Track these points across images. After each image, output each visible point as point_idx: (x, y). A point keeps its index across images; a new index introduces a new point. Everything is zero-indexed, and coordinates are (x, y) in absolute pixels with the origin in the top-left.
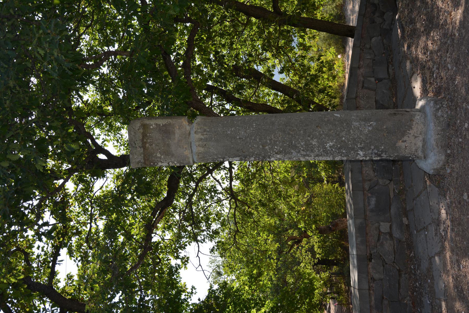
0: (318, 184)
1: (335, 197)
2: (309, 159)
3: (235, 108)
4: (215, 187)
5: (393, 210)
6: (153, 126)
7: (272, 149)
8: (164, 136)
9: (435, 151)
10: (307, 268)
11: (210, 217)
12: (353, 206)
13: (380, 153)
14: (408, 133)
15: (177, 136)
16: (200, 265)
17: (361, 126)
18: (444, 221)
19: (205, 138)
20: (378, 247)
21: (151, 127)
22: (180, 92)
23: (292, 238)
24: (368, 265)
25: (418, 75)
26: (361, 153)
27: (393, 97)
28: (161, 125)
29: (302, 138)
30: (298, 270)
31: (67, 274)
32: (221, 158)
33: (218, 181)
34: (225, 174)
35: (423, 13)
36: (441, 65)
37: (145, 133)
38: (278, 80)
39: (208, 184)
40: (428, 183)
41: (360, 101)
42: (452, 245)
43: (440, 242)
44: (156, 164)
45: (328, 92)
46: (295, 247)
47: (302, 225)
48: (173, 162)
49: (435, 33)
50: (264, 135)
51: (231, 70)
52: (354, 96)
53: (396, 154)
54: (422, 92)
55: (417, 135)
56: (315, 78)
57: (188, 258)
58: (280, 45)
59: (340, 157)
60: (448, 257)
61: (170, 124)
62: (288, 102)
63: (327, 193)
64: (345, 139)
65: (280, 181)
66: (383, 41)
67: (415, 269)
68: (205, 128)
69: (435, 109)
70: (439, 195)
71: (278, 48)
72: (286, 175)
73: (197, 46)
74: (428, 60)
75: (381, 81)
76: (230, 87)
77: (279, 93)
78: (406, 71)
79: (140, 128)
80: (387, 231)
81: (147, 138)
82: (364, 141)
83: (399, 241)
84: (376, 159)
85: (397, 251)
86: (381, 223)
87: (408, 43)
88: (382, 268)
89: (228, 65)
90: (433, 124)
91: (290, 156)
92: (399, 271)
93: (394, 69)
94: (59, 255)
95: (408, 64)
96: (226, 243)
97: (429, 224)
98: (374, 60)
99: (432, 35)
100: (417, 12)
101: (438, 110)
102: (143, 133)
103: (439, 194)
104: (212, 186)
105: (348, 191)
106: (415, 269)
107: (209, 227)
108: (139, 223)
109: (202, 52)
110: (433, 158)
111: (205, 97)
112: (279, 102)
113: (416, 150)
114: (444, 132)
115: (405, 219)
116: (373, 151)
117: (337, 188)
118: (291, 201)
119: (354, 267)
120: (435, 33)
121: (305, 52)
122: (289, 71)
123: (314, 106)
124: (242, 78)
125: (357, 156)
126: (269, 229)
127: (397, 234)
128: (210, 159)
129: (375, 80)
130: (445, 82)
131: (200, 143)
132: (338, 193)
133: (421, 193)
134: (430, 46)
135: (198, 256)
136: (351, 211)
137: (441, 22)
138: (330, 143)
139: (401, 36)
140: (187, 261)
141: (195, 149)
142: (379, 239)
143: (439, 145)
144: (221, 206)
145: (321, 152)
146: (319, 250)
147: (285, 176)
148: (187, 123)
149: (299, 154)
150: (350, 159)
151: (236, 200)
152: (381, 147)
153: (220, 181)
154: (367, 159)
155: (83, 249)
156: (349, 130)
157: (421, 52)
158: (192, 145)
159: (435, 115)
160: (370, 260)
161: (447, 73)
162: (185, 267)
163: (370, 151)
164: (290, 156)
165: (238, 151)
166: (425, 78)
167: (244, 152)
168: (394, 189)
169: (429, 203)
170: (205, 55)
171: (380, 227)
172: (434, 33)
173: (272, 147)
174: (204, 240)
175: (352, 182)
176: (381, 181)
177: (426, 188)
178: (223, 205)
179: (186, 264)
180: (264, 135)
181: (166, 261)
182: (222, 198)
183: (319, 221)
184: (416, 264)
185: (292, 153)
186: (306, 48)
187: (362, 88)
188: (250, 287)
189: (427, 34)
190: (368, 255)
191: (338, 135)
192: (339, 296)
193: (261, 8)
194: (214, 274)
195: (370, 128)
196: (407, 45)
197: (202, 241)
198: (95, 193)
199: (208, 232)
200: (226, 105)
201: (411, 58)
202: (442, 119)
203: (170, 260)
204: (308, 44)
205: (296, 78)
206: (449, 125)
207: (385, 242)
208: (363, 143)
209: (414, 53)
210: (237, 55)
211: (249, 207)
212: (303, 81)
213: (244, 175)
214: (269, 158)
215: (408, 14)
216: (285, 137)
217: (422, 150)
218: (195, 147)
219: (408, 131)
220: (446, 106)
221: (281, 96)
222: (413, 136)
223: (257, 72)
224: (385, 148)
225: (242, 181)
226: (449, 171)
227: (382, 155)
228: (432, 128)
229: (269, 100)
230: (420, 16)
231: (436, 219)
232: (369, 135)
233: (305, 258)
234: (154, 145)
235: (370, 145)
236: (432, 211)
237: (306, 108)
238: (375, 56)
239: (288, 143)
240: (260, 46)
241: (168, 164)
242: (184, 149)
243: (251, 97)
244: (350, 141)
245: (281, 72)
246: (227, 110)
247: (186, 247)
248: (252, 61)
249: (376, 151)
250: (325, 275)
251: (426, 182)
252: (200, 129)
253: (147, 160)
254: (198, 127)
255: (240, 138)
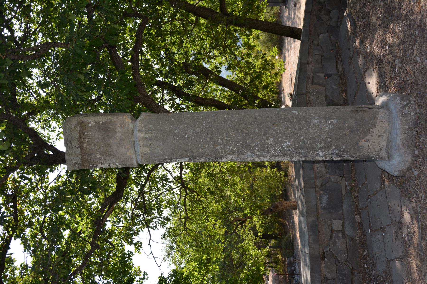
0: (258, 169)
1: (274, 181)
2: (264, 160)
3: (185, 102)
4: (166, 176)
5: (345, 207)
6: (91, 124)
7: (224, 149)
8: (104, 135)
9: (400, 151)
10: (249, 245)
11: (163, 203)
12: (304, 204)
13: (342, 153)
14: (372, 131)
15: (118, 134)
16: (151, 253)
17: (321, 124)
18: (408, 226)
19: (149, 137)
20: (331, 245)
21: (90, 125)
22: (123, 87)
23: (237, 219)
24: (321, 264)
25: (374, 70)
26: (321, 153)
27: (343, 93)
28: (101, 123)
29: (256, 137)
30: (242, 247)
31: (20, 264)
32: (168, 159)
33: (169, 172)
34: (176, 164)
35: (380, 6)
36: (405, 59)
37: (82, 132)
38: (225, 77)
39: (160, 173)
40: (386, 183)
41: (311, 97)
42: (422, 254)
43: (402, 246)
44: (95, 166)
45: (272, 88)
46: (240, 226)
47: (248, 211)
48: (114, 164)
49: (396, 26)
50: (215, 134)
51: (181, 67)
52: (304, 92)
53: (358, 155)
54: (379, 88)
55: (381, 134)
56: (259, 76)
57: (141, 243)
58: (226, 44)
59: (298, 157)
60: (414, 265)
61: (111, 121)
62: (235, 98)
63: (267, 177)
64: (304, 138)
65: (227, 170)
66: (330, 38)
67: (368, 268)
68: (150, 126)
69: (401, 106)
70: (401, 197)
71: (225, 47)
72: (232, 164)
73: (146, 41)
74: (386, 55)
75: (331, 77)
76: (180, 83)
77: (226, 89)
78: (359, 66)
79: (76, 126)
80: (339, 229)
81: (84, 137)
82: (324, 141)
83: (352, 239)
84: (336, 159)
85: (350, 249)
86: (334, 221)
87: (361, 38)
88: (335, 267)
89: (178, 62)
90: (399, 122)
91: (243, 157)
92: (352, 269)
93: (343, 64)
94: (9, 248)
95: (361, 61)
96: (177, 229)
97: (388, 225)
98: (323, 56)
99: (392, 27)
100: (371, 6)
101: (405, 107)
102: (80, 131)
103: (401, 196)
104: (164, 175)
105: (299, 187)
106: (368, 268)
107: (160, 213)
108: (86, 220)
109: (151, 47)
110: (398, 159)
111: (156, 91)
112: (226, 97)
113: (380, 150)
114: (411, 131)
115: (357, 217)
116: (333, 151)
117: (275, 172)
118: (237, 188)
119: (306, 264)
120: (396, 26)
121: (250, 51)
122: (235, 68)
123: (259, 100)
124: (192, 74)
125: (316, 156)
126: (217, 215)
127: (349, 232)
128: (156, 160)
129: (325, 76)
130: (411, 77)
131: (145, 142)
132: (277, 177)
133: (378, 192)
134: (389, 38)
135: (149, 244)
136: (302, 208)
137: (405, 13)
138: (287, 143)
139: (352, 32)
140: (140, 246)
141: (139, 150)
142: (331, 237)
143: (405, 145)
144: (172, 193)
145: (277, 152)
146: (260, 228)
147: (231, 166)
148: (130, 121)
149: (254, 154)
150: (308, 160)
151: (186, 188)
152: (342, 146)
153: (171, 170)
154: (326, 160)
155: (38, 238)
156: (308, 129)
157: (378, 46)
158: (136, 145)
159: (402, 113)
160: (323, 259)
161: (413, 67)
162: (138, 252)
163: (330, 152)
164: (243, 157)
165: (186, 151)
166: (383, 73)
167: (193, 153)
168: (346, 186)
169: (388, 203)
170: (154, 50)
171: (333, 224)
172: (395, 25)
173: (224, 147)
174: (156, 227)
175: (304, 179)
176: (333, 178)
177: (384, 187)
178: (174, 193)
179: (139, 249)
180: (215, 134)
181: (120, 246)
182: (173, 187)
183: (263, 207)
184: (370, 263)
185: (246, 153)
186: (250, 47)
187: (312, 83)
188: (199, 272)
189: (385, 27)
190: (321, 253)
191: (297, 134)
192: (277, 265)
193: (209, 10)
194: (167, 248)
195: (330, 127)
196: (360, 40)
197: (154, 228)
198: (50, 184)
199: (160, 219)
200: (176, 100)
201: (364, 53)
202: (409, 117)
203: (124, 245)
204: (253, 44)
205: (242, 75)
206: (416, 124)
207: (337, 241)
208: (323, 142)
209: (369, 47)
210: (186, 53)
211: (198, 195)
212: (249, 79)
213: (193, 165)
214: (221, 159)
215: (360, 8)
216: (239, 136)
217: (386, 150)
218: (139, 147)
219: (371, 130)
220: (414, 103)
221: (227, 92)
222: (377, 135)
223: (205, 68)
224: (346, 147)
225: (192, 170)
226: (416, 173)
227: (344, 155)
228: (398, 126)
229: (216, 95)
230: (376, 9)
231: (397, 221)
232: (330, 134)
233: (248, 236)
234: (93, 145)
235: (331, 145)
236: (391, 212)
237: (251, 103)
238: (324, 52)
239: (241, 143)
240: (208, 46)
241: (109, 165)
242: (127, 149)
243: (200, 92)
244: (309, 141)
245: (228, 69)
246: (178, 104)
247: (139, 233)
248: (201, 58)
249: (337, 152)
250: (265, 250)
251: (384, 181)
252: (144, 127)
253: (86, 161)
254: (142, 125)
255: (188, 137)
